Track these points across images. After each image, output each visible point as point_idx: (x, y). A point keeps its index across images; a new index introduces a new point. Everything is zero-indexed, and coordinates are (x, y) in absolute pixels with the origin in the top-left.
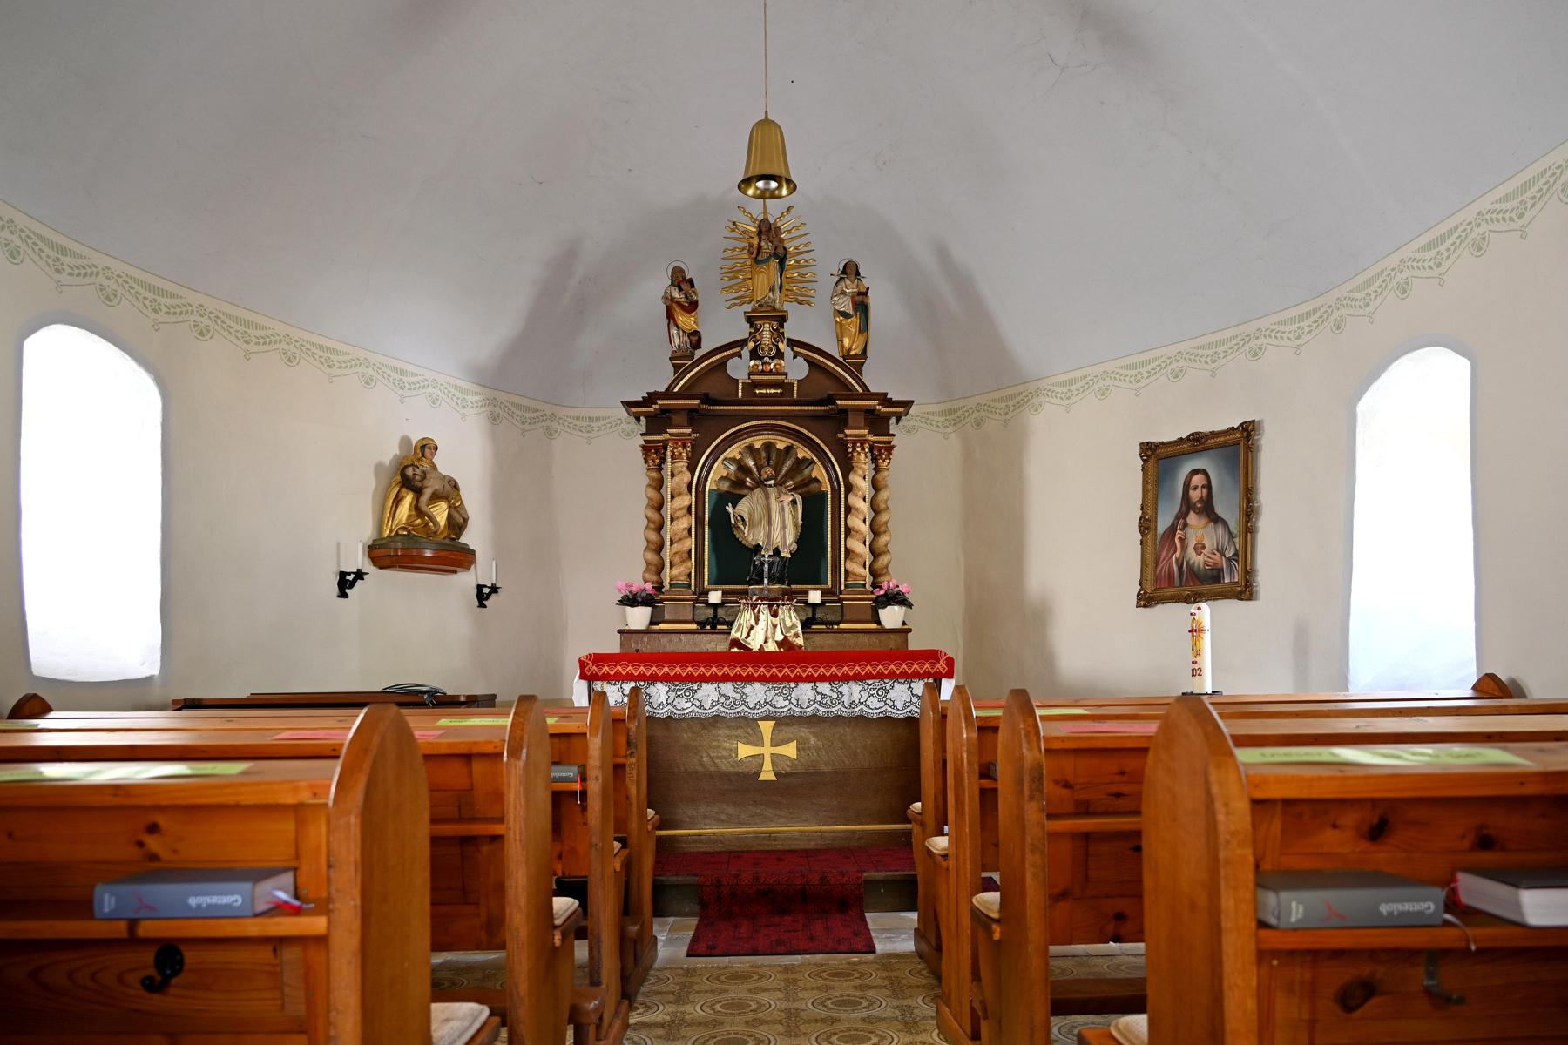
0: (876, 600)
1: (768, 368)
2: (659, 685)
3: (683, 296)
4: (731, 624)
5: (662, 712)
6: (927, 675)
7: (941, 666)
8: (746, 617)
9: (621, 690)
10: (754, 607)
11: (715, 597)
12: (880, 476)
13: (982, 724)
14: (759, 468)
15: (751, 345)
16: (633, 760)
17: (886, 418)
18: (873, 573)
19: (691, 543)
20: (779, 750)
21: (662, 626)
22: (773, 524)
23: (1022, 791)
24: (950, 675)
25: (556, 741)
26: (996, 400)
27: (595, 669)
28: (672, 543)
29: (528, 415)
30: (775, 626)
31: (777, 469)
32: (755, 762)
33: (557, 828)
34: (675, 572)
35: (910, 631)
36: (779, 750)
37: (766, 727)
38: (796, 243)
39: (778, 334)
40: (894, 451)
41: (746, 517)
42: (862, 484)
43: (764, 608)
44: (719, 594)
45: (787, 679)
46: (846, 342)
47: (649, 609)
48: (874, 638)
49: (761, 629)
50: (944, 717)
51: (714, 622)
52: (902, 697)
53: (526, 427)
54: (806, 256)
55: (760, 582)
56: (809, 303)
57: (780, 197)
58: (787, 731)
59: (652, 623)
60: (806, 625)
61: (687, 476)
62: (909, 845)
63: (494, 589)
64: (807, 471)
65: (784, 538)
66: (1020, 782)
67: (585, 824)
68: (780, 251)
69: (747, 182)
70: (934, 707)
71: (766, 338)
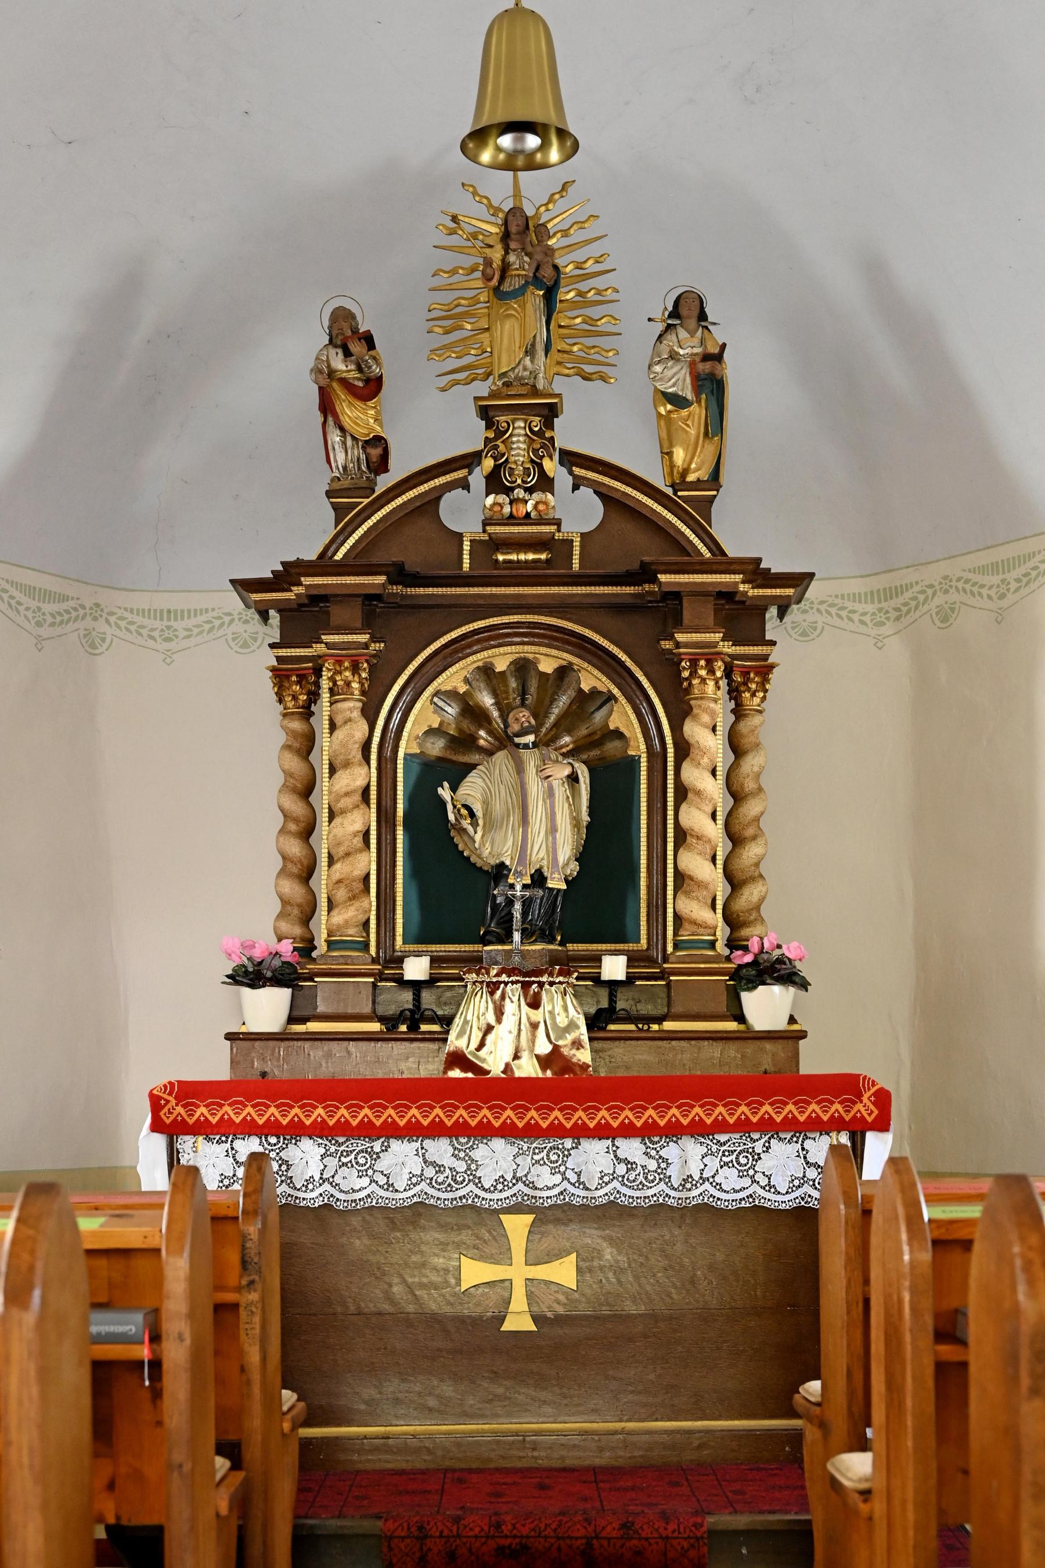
0: (736, 974)
1: (521, 510)
2: (306, 1143)
3: (352, 366)
5: (313, 1197)
6: (836, 1124)
7: (866, 1108)
8: (477, 1009)
9: (232, 1154)
10: (493, 987)
11: (416, 968)
12: (744, 726)
13: (938, 1234)
15: (488, 464)
16: (254, 1296)
17: (759, 610)
18: (731, 920)
19: (368, 861)
20: (541, 1272)
21: (313, 1026)
22: (531, 822)
23: (1015, 1380)
24: (882, 1125)
25: (102, 1262)
26: (982, 570)
27: (180, 1110)
28: (331, 861)
29: (47, 608)
30: (534, 1026)
31: (539, 713)
32: (494, 1295)
33: (103, 1428)
34: (338, 918)
35: (802, 1035)
36: (541, 1272)
37: (517, 1226)
38: (579, 255)
39: (542, 441)
42: (708, 739)
43: (514, 991)
45: (557, 1131)
46: (679, 455)
47: (286, 993)
48: (732, 1051)
50: (867, 1213)
51: (415, 1017)
52: (786, 1169)
53: (45, 632)
54: (599, 282)
55: (507, 938)
56: (604, 379)
57: (545, 166)
58: (558, 1235)
59: (292, 1020)
60: (595, 1022)
62: (797, 1460)
64: (599, 716)
65: (553, 851)
66: (1012, 1359)
67: (159, 1423)
68: (547, 273)
69: (479, 136)
70: (849, 1196)
71: (519, 451)
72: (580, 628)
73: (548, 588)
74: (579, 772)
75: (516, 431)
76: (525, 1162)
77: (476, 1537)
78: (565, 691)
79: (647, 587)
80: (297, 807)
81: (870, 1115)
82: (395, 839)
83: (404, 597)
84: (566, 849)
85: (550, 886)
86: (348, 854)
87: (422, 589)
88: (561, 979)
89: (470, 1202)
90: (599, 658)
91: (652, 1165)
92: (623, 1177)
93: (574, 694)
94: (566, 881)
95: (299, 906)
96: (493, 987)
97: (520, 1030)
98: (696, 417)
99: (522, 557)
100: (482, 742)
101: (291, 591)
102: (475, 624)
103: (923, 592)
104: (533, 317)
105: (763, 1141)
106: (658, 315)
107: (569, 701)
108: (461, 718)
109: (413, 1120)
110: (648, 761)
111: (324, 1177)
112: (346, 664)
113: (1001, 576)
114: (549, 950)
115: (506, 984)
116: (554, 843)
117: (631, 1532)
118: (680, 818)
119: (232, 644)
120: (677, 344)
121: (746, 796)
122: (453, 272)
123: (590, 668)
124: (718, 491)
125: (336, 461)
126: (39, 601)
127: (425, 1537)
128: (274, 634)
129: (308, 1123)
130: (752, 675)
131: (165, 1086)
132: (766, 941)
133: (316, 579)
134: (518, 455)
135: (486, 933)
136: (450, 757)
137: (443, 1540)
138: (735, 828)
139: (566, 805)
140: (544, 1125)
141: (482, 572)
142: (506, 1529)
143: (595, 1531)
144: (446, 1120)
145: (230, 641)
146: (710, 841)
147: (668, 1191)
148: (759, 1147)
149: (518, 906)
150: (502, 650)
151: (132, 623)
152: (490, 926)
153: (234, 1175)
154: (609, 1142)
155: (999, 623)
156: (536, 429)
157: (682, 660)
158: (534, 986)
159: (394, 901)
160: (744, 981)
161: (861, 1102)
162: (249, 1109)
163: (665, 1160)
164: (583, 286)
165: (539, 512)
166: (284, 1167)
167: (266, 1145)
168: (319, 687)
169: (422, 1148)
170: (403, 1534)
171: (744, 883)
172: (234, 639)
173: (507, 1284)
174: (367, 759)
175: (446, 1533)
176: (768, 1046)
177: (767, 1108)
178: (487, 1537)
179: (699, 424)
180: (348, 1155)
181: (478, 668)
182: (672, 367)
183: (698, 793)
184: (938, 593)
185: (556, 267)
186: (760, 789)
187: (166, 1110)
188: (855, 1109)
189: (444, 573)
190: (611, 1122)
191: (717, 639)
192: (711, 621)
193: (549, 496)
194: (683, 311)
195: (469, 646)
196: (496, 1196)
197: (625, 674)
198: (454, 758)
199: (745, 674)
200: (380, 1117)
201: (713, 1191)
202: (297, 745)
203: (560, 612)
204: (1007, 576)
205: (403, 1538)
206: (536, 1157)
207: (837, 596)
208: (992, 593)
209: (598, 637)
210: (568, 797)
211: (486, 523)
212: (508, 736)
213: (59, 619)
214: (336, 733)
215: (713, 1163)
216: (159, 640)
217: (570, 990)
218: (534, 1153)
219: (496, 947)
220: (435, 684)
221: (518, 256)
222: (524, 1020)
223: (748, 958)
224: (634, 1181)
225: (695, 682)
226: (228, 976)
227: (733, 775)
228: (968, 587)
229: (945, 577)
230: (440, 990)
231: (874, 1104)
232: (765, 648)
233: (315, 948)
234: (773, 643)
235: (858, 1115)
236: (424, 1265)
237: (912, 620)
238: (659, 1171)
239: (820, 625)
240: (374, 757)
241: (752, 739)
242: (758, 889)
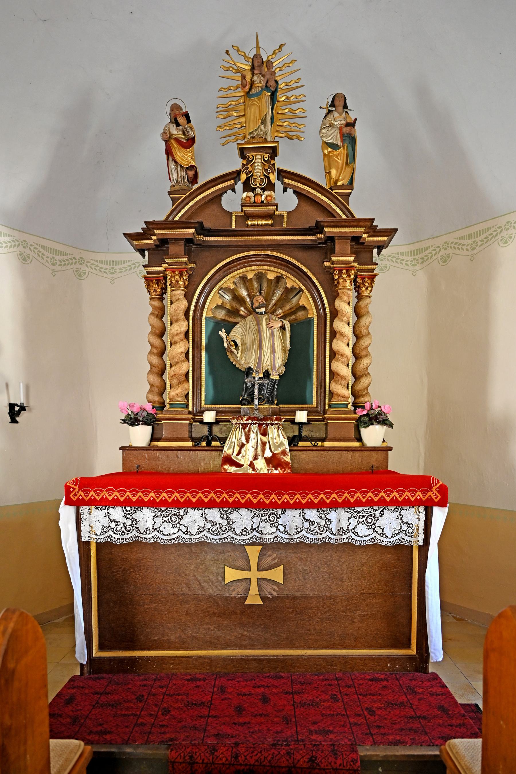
1: (259, 199)
2: (145, 510)
3: (180, 135)
4: (223, 441)
5: (149, 537)
6: (418, 503)
7: (434, 494)
8: (237, 436)
10: (244, 426)
11: (209, 417)
12: (362, 304)
14: (251, 297)
15: (244, 177)
19: (187, 366)
21: (161, 444)
22: (263, 349)
24: (442, 503)
26: (464, 238)
29: (57, 258)
30: (264, 444)
37: (253, 552)
39: (269, 164)
40: (377, 278)
41: (240, 344)
42: (346, 307)
43: (255, 428)
44: (213, 413)
45: (274, 505)
46: (334, 172)
47: (150, 427)
49: (252, 449)
51: (209, 439)
54: (296, 92)
55: (251, 402)
56: (298, 138)
60: (293, 441)
61: (184, 304)
63: (23, 408)
64: (295, 300)
65: (273, 362)
68: (272, 83)
71: (258, 170)
72: (287, 257)
73: (272, 237)
74: (286, 325)
75: (257, 160)
76: (257, 520)
77: (223, 764)
79: (318, 236)
80: (157, 342)
81: (436, 498)
82: (201, 356)
83: (204, 242)
84: (279, 362)
85: (272, 378)
86: (178, 363)
87: (213, 238)
88: (276, 422)
89: (229, 541)
91: (323, 523)
92: (308, 529)
93: (283, 290)
94: (280, 376)
95: (157, 387)
96: (244, 426)
97: (257, 446)
98: (342, 155)
99: (260, 222)
100: (242, 313)
101: (151, 239)
103: (435, 250)
104: (265, 105)
105: (380, 510)
106: (324, 105)
108: (232, 301)
109: (200, 499)
110: (318, 320)
111: (155, 528)
113: (473, 240)
114: (272, 408)
115: (251, 424)
117: (315, 764)
118: (333, 346)
120: (333, 119)
122: (228, 89)
123: (291, 277)
124: (352, 190)
125: (173, 177)
126: (53, 254)
127: (194, 763)
128: (146, 260)
129: (146, 500)
130: (366, 279)
131: (73, 481)
133: (161, 231)
134: (258, 172)
135: (243, 400)
137: (204, 765)
138: (357, 351)
139: (280, 340)
140: (267, 502)
141: (240, 228)
142: (241, 759)
143: (293, 763)
144: (216, 499)
145: (138, 274)
146: (347, 357)
147: (330, 536)
148: (377, 514)
149: (257, 388)
150: (251, 268)
151: (97, 266)
152: (244, 396)
153: (109, 526)
154: (301, 511)
155: (472, 261)
156: (266, 159)
158: (264, 425)
159: (201, 385)
160: (362, 423)
161: (432, 491)
162: (116, 493)
163: (329, 520)
164: (289, 94)
165: (268, 200)
166: (134, 523)
167: (125, 511)
168: (167, 286)
169: (205, 513)
170: (181, 761)
171: (361, 376)
172: (140, 273)
173: (248, 581)
174: (188, 319)
175: (205, 761)
176: (374, 454)
177: (382, 494)
178: (230, 764)
179: (344, 158)
180: (167, 516)
181: (240, 277)
182: (331, 130)
183: (342, 334)
184: (442, 250)
185: (276, 82)
187: (73, 493)
188: (428, 495)
189: (223, 229)
190: (302, 501)
193: (273, 193)
194: (337, 103)
195: (235, 266)
196: (242, 538)
197: (307, 279)
198: (229, 320)
199: (363, 279)
200: (183, 497)
201: (353, 536)
202: (156, 313)
203: (277, 250)
204: (476, 239)
205: (181, 763)
206: (263, 518)
207: (395, 254)
208: (469, 248)
210: (280, 337)
211: (242, 206)
212: (253, 309)
213: (63, 263)
215: (354, 522)
216: (108, 274)
217: (281, 427)
218: (262, 516)
219: (247, 406)
220: (220, 284)
221: (258, 77)
222: (259, 441)
223: (365, 412)
224: (313, 531)
225: (341, 281)
226: (122, 420)
227: (356, 326)
228: (456, 246)
229: (445, 243)
230: (221, 426)
231: (438, 492)
232: (372, 266)
233: (166, 406)
235: (430, 498)
236: (206, 570)
237: (429, 263)
238: (326, 526)
240: (191, 318)
241: (365, 309)
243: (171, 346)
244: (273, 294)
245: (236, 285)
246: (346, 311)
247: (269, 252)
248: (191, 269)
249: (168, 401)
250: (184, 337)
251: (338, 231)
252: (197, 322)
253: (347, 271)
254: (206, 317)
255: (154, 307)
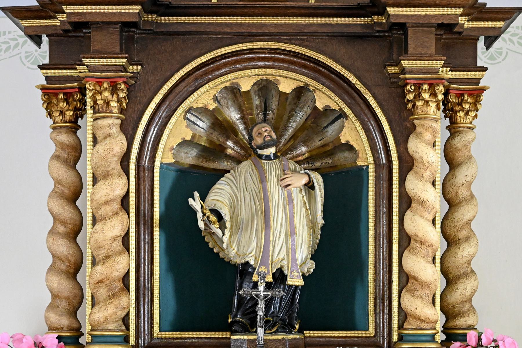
12: (458, 142)
19: (126, 263)
31: (279, 128)
34: (100, 314)
40: (485, 96)
41: (227, 217)
42: (427, 151)
61: (119, 143)
64: (331, 131)
65: (292, 252)
74: (315, 181)
78: (302, 108)
79: (376, 18)
82: (152, 239)
84: (303, 251)
86: (108, 257)
90: (332, 80)
93: (309, 111)
100: (229, 151)
102: (223, 49)
107: (305, 117)
108: (211, 131)
110: (375, 171)
112: (106, 85)
114: (292, 339)
116: (293, 245)
119: (26, 62)
121: (460, 203)
123: (324, 89)
130: (466, 97)
132: (483, 337)
133: (76, 7)
136: (202, 164)
138: (450, 231)
139: (303, 210)
149: (261, 305)
150: (247, 72)
157: (407, 84)
168: (85, 104)
171: (458, 278)
172: (26, 57)
174: (126, 170)
181: (226, 88)
183: (422, 203)
186: (472, 196)
191: (439, 66)
192: (433, 50)
195: (218, 69)
198: (206, 165)
199: (460, 95)
202: (64, 155)
209: (332, 62)
210: (305, 203)
212: (252, 147)
214: (97, 146)
225: (419, 104)
227: (448, 184)
232: (477, 73)
234: (484, 69)
239: (504, 52)
242: (471, 284)
243: (94, 224)
244: (290, 117)
245: (219, 102)
246: (429, 159)
247: (283, 44)
248: (135, 76)
249: (88, 328)
250: (119, 206)
251: (413, 13)
252: (144, 173)
253: (431, 85)
254: (162, 164)
255: (60, 145)
